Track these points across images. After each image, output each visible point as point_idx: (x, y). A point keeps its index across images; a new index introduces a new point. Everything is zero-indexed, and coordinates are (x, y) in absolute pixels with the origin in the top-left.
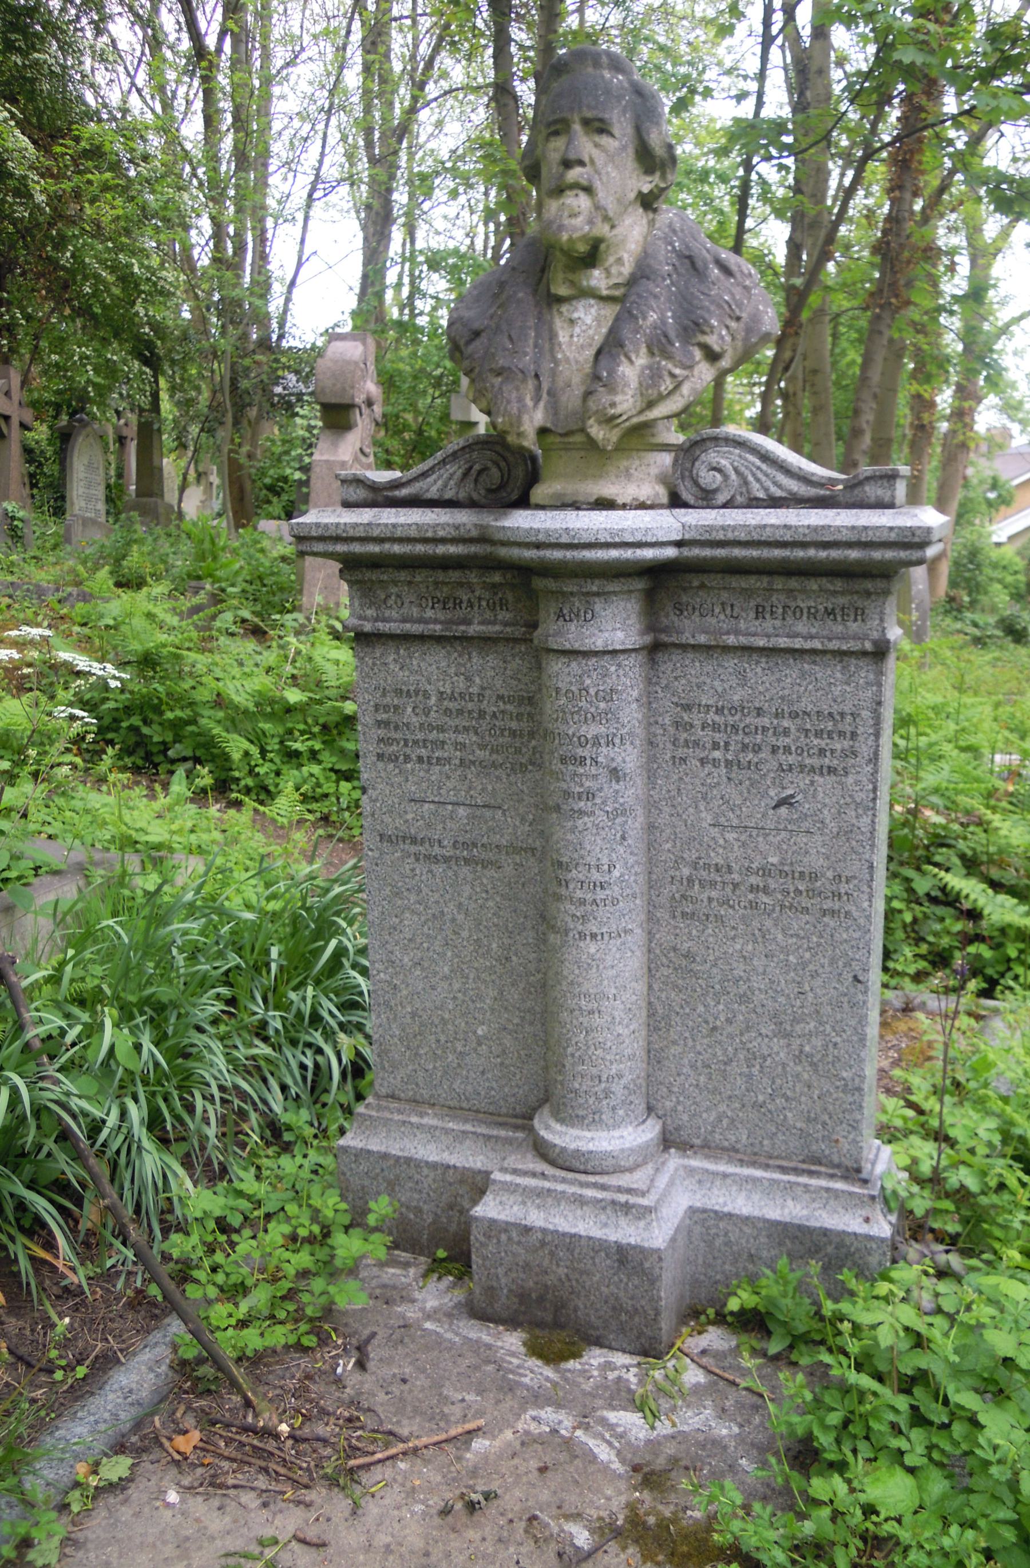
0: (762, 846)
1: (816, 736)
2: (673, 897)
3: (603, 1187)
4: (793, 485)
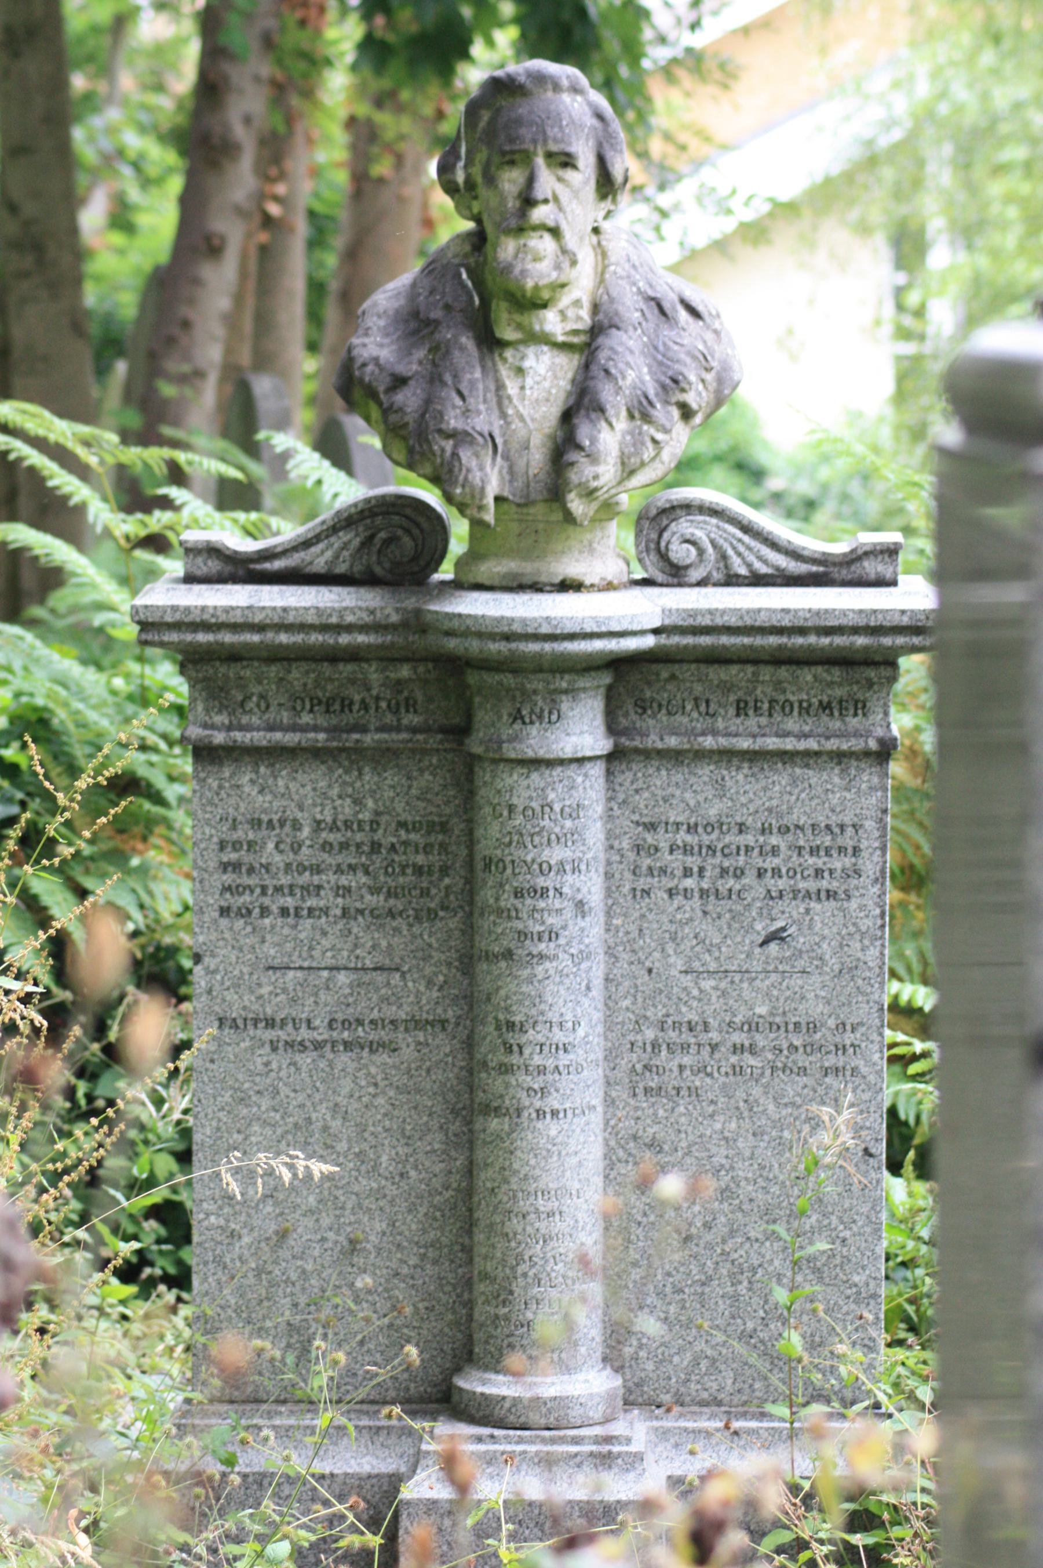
0: (747, 994)
1: (811, 854)
2: (633, 1069)
3: (576, 1441)
4: (782, 561)
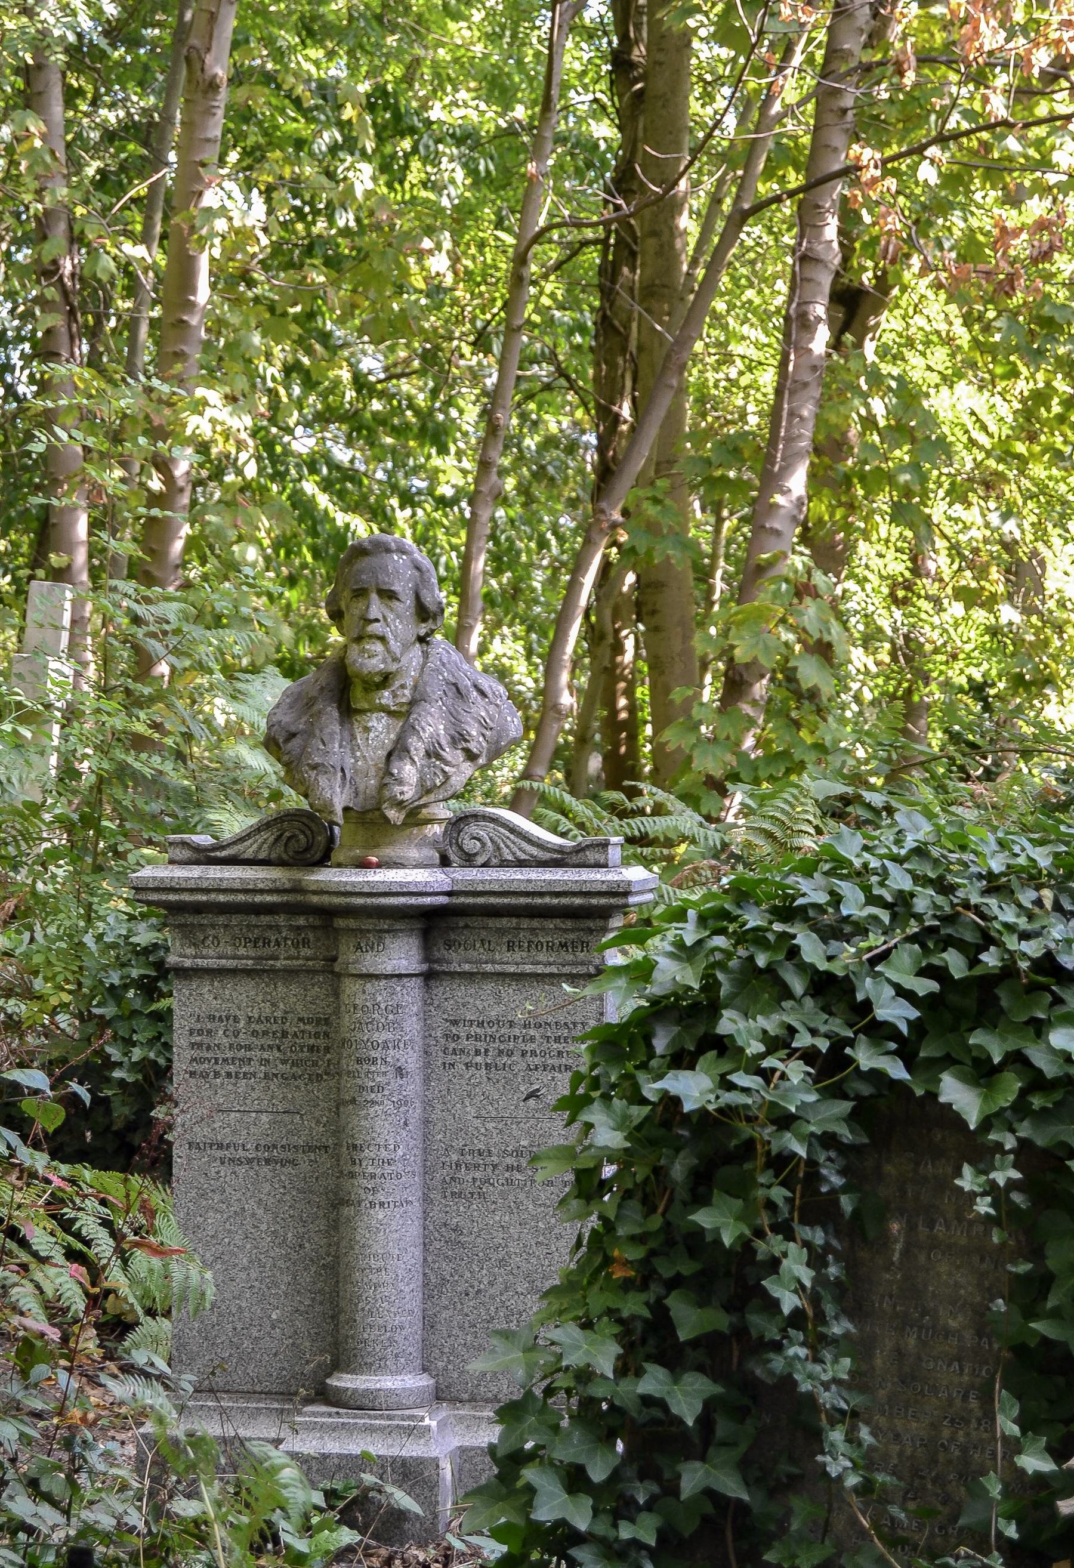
4: (535, 851)
